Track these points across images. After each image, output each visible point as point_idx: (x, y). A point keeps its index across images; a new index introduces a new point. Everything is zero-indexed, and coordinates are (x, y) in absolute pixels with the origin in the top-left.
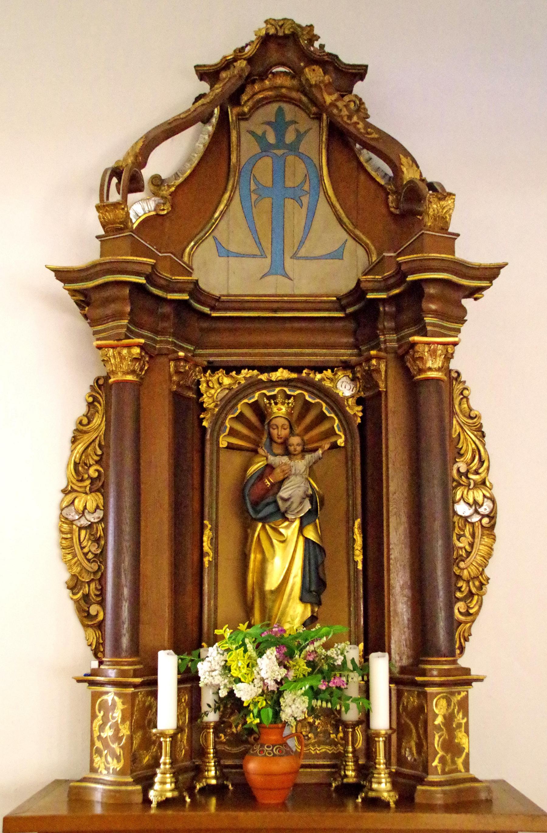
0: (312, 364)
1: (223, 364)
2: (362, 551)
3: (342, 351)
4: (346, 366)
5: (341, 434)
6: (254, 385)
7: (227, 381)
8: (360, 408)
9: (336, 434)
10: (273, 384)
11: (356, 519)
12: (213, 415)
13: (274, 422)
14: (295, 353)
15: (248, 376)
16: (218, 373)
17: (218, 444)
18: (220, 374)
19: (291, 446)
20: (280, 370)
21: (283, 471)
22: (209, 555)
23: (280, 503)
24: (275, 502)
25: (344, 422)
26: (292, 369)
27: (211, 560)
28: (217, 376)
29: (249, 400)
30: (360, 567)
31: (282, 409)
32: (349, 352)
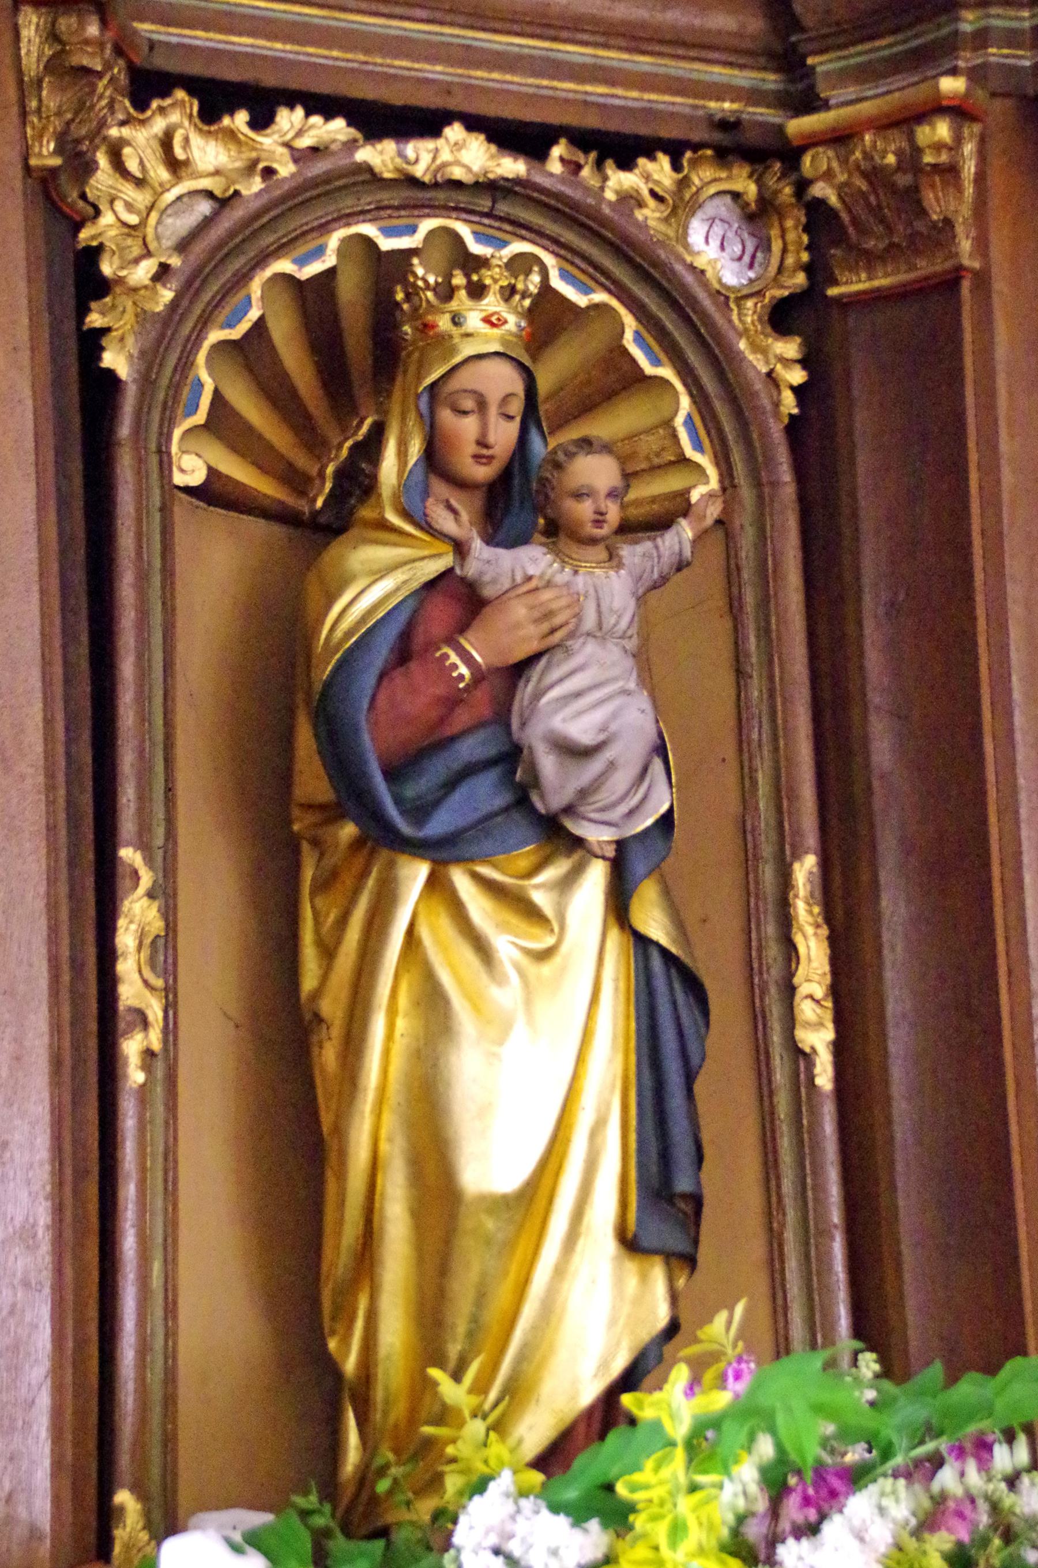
0: (592, 121)
1: (196, 68)
2: (829, 1004)
3: (718, 73)
4: (731, 144)
5: (703, 460)
6: (323, 192)
7: (208, 154)
8: (790, 348)
9: (683, 461)
10: (416, 194)
11: (797, 856)
12: (143, 317)
13: (465, 379)
14: (520, 57)
15: (305, 142)
16: (162, 110)
17: (165, 464)
18: (176, 113)
19: (578, 496)
20: (455, 132)
21: (549, 615)
22: (145, 1024)
23: (548, 764)
24: (512, 757)
25: (721, 408)
26: (506, 135)
27: (156, 1045)
28: (159, 125)
29: (301, 262)
30: (824, 1078)
31: (506, 322)
32: (743, 78)
